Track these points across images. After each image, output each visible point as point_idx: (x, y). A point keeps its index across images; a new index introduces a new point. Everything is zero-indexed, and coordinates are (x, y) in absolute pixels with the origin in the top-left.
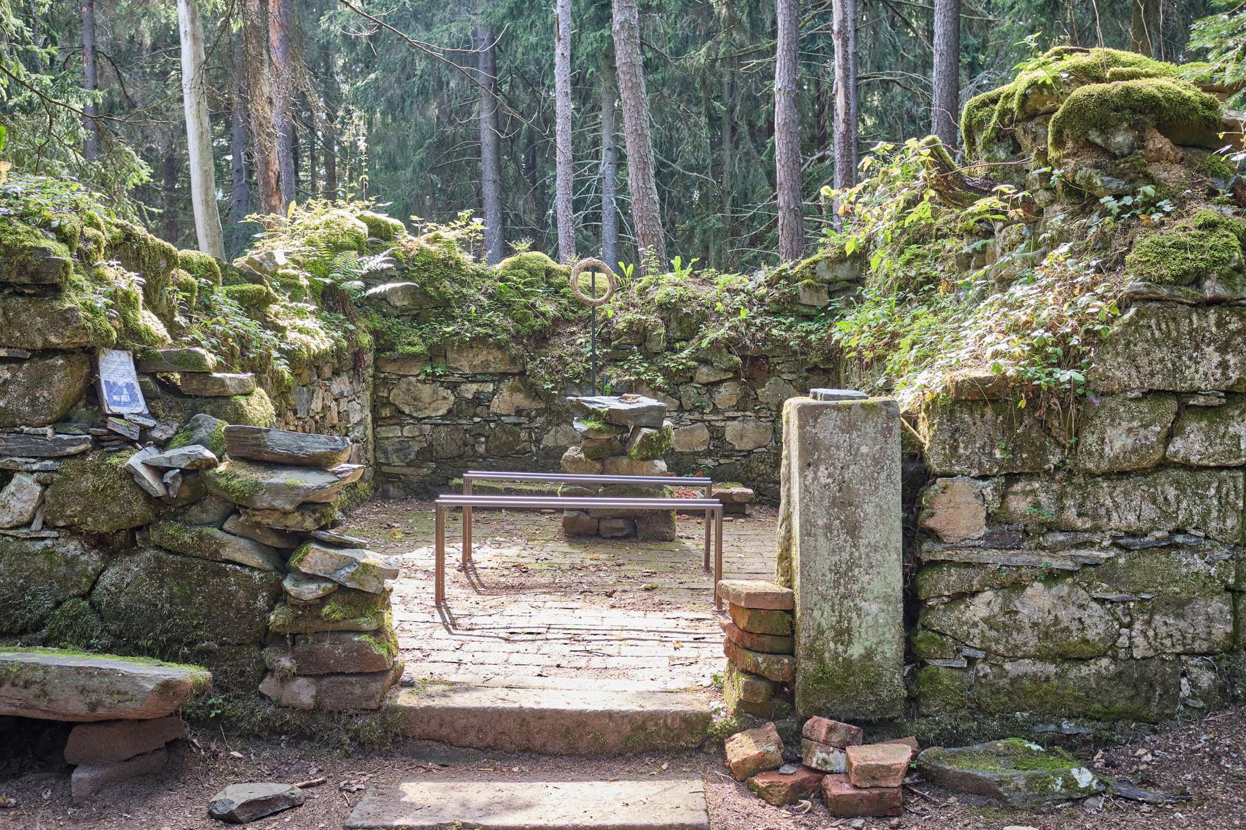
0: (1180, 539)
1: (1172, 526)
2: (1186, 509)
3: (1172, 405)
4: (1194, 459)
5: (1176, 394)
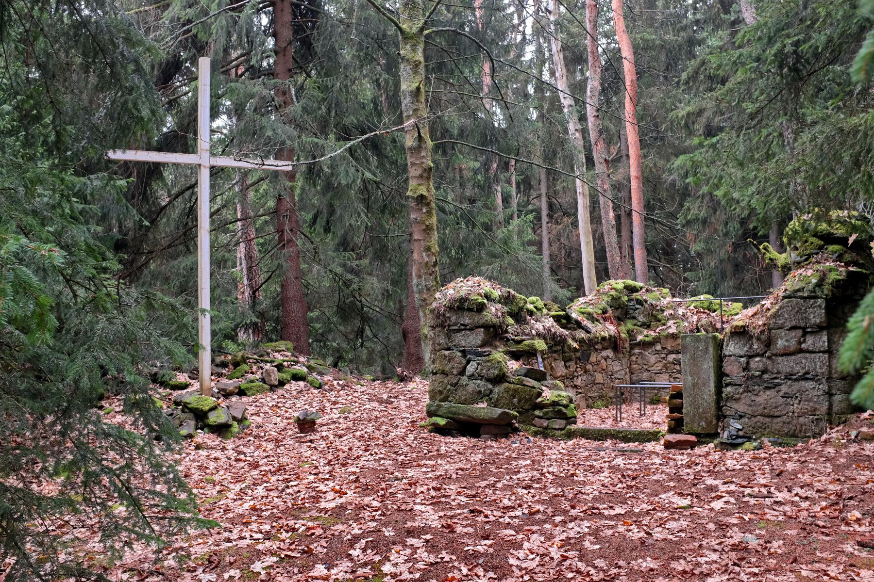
0: (808, 376)
2: (808, 366)
5: (800, 328)
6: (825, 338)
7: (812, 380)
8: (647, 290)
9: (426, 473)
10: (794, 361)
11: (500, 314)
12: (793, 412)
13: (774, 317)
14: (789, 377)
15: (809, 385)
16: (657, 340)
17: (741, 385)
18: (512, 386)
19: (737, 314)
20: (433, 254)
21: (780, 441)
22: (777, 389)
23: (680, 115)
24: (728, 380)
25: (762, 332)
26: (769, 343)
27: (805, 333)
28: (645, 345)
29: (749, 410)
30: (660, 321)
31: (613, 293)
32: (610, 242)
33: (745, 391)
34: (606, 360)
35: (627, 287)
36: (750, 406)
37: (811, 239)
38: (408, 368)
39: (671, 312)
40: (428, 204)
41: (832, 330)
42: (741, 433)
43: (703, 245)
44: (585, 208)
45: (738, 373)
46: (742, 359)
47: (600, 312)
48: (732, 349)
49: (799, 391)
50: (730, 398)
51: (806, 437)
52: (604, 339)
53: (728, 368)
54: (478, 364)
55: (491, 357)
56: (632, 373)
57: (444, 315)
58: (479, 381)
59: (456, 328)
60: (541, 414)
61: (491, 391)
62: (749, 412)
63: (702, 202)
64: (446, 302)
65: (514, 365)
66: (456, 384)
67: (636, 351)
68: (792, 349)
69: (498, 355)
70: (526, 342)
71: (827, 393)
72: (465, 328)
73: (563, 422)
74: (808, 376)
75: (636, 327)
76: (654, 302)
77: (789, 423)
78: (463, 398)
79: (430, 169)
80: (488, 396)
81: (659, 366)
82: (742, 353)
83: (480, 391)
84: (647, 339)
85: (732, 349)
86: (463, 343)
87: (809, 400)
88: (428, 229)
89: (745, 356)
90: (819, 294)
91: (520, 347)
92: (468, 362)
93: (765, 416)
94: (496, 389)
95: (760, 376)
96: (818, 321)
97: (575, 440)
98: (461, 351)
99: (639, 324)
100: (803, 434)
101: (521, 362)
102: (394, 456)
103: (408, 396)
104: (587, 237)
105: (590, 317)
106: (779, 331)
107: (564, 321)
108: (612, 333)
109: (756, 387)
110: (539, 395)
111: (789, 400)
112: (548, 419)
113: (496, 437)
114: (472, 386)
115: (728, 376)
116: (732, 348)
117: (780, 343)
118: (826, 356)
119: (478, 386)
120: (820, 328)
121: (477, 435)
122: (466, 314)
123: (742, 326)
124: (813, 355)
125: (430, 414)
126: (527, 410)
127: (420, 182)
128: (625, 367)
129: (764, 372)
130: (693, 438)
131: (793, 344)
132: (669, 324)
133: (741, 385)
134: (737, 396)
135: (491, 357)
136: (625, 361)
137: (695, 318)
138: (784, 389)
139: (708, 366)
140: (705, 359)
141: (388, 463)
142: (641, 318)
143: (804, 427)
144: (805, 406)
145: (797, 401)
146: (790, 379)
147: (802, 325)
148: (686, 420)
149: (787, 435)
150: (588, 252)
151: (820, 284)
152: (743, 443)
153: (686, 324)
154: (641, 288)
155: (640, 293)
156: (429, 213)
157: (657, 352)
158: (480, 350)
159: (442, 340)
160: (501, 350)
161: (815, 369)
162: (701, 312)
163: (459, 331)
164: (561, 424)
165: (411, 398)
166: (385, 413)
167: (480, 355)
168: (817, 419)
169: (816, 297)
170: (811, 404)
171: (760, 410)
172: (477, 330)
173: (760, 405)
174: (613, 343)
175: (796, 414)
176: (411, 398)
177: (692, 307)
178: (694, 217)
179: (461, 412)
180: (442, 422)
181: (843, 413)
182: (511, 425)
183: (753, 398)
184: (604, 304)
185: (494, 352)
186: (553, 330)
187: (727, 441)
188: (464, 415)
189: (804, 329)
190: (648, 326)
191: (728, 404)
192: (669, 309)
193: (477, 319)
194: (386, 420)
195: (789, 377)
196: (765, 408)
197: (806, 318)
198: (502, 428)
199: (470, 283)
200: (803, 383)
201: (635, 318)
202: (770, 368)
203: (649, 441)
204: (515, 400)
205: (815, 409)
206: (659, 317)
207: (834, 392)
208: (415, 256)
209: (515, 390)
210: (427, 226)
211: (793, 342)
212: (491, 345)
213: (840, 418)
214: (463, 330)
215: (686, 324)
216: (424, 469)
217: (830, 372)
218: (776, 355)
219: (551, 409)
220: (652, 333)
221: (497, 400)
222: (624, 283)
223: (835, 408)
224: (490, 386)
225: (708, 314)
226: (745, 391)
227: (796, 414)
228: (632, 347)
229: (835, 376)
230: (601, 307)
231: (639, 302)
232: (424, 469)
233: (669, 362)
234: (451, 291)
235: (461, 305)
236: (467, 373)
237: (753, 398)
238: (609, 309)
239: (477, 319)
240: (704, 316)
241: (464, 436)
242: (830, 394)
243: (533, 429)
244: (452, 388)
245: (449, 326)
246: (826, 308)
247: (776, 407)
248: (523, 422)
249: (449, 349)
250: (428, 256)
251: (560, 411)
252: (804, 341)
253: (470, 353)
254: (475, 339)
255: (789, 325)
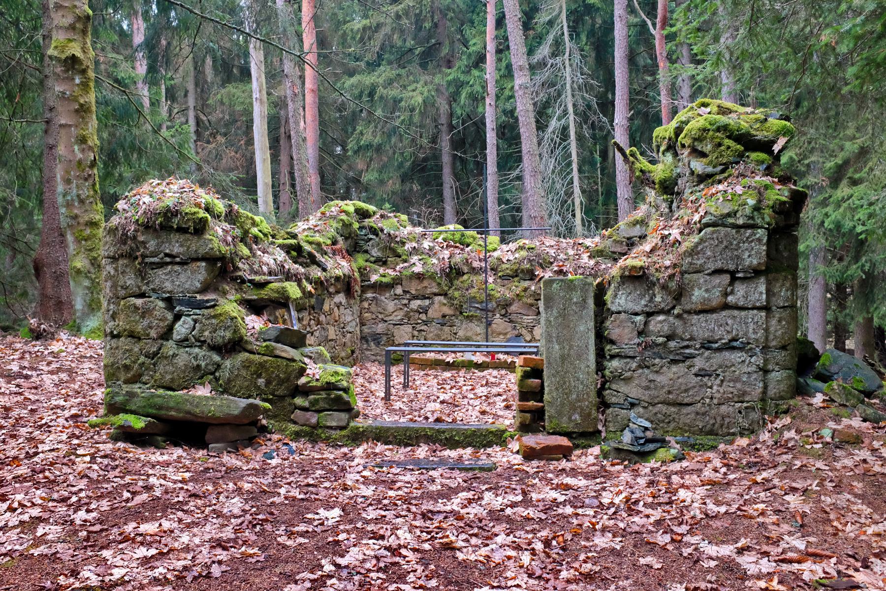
0: (735, 344)
1: (730, 337)
2: (736, 329)
3: (728, 276)
4: (741, 303)
5: (727, 271)
6: (763, 288)
7: (741, 349)
8: (382, 216)
9: (146, 562)
10: (716, 321)
11: (230, 239)
12: (712, 398)
13: (691, 255)
14: (707, 345)
15: (736, 357)
16: (397, 281)
17: (633, 358)
18: (256, 358)
19: (495, 250)
20: (91, 148)
21: (692, 441)
22: (687, 363)
23: (356, 28)
24: (615, 350)
25: (672, 277)
26: (679, 295)
27: (734, 279)
28: (381, 287)
29: (645, 396)
30: (400, 257)
31: (343, 217)
33: (640, 367)
34: (338, 307)
35: (358, 211)
36: (647, 388)
37: (728, 142)
38: (46, 318)
39: (414, 244)
40: (84, 72)
41: (771, 276)
42: (649, 434)
43: (376, 175)
44: (262, 117)
45: (630, 339)
46: (638, 318)
47: (329, 242)
48: (622, 302)
49: (720, 367)
50: (618, 377)
51: (729, 434)
53: (613, 329)
54: (195, 321)
55: (219, 310)
56: (362, 324)
57: (135, 238)
58: (197, 350)
59: (156, 260)
60: (306, 404)
61: (219, 366)
62: (646, 398)
63: (376, 127)
64: (138, 215)
65: (254, 323)
66: (155, 354)
67: (369, 295)
68: (714, 303)
69: (230, 305)
70: (271, 285)
71: (761, 369)
72: (172, 259)
73: (344, 416)
74: (735, 344)
75: (368, 264)
76: (392, 232)
77: (704, 414)
78: (168, 377)
79: (88, 17)
80: (213, 373)
81: (400, 315)
82: (638, 309)
83: (198, 366)
84: (384, 280)
85: (622, 302)
86: (168, 286)
87: (737, 380)
88: (83, 110)
89: (643, 312)
90: (759, 221)
91: (264, 293)
92: (177, 317)
93: (669, 404)
94: (228, 363)
95: (664, 345)
96: (755, 262)
97: (365, 446)
98: (163, 300)
99: (372, 259)
100: (725, 430)
101: (265, 317)
102: (62, 509)
103: (54, 366)
104: (264, 153)
106: (695, 276)
107: (294, 253)
108: (346, 271)
109: (657, 361)
110: (302, 372)
111: (706, 379)
112: (318, 411)
113: (235, 447)
114: (184, 358)
115: (612, 342)
116: (620, 300)
117: (698, 295)
118: (763, 314)
119: (196, 358)
120: (757, 273)
121: (203, 445)
122: (174, 237)
123: (642, 268)
124: (743, 313)
125: (114, 408)
126: (282, 398)
127: (70, 35)
128: (355, 316)
129: (670, 338)
130: (564, 441)
131: (716, 297)
132: (412, 261)
133: (633, 358)
134: (629, 374)
135: (219, 310)
136: (356, 308)
137: (446, 254)
138: (699, 363)
139: (586, 327)
140: (581, 317)
141: (53, 531)
142: (375, 253)
143: (727, 420)
144: (729, 388)
145: (718, 382)
146: (708, 349)
147: (732, 267)
148: (549, 411)
149: (701, 431)
150: (264, 172)
151: (757, 208)
152: (653, 452)
153: (435, 261)
154: (374, 213)
156: (85, 86)
157: (397, 297)
158: (199, 297)
159: (130, 280)
160: (232, 298)
161: (746, 334)
163: (162, 265)
164: (340, 420)
165: (59, 370)
166: (20, 398)
167: (200, 305)
168: (746, 408)
169: (754, 227)
170: (739, 385)
171: (662, 394)
172: (194, 265)
173: (663, 387)
174: (346, 285)
175: (715, 401)
176: (59, 370)
177: (440, 240)
179: (172, 404)
180: (138, 423)
181: (782, 398)
182: (255, 423)
183: (651, 376)
185: (221, 301)
186: (287, 267)
187: (631, 448)
188: (178, 410)
189: (733, 274)
191: (614, 387)
193: (195, 246)
194: (24, 413)
195: (707, 345)
196: (669, 392)
197: (738, 257)
198: (244, 432)
199: (175, 187)
200: (727, 354)
201: (366, 252)
202: (679, 331)
203: (489, 445)
204: (261, 381)
205: (745, 393)
206: (399, 251)
207: (770, 367)
208: (61, 150)
209: (262, 365)
210: (82, 105)
211: (717, 293)
212: (216, 290)
213: (777, 405)
214: (167, 264)
215: (435, 261)
216: (142, 552)
217: (767, 338)
218: (689, 312)
219: (324, 395)
220: (390, 272)
221: (229, 381)
223: (771, 392)
224: (216, 358)
225: (462, 250)
226: (640, 367)
227: (715, 401)
228: (364, 289)
229: (774, 343)
230: (329, 235)
231: (374, 231)
232: (142, 552)
233: (412, 310)
234: (147, 199)
235: (166, 222)
236: (176, 336)
237: (651, 376)
238: (340, 239)
239: (195, 246)
240: (458, 251)
241: (176, 444)
242: (765, 371)
243: (293, 428)
244: (148, 361)
245: (144, 256)
246: (768, 243)
247: (686, 391)
248: (274, 417)
249: (142, 295)
250: (83, 151)
251: (339, 399)
252: (732, 293)
253: (181, 302)
254: (190, 279)
255: (712, 266)
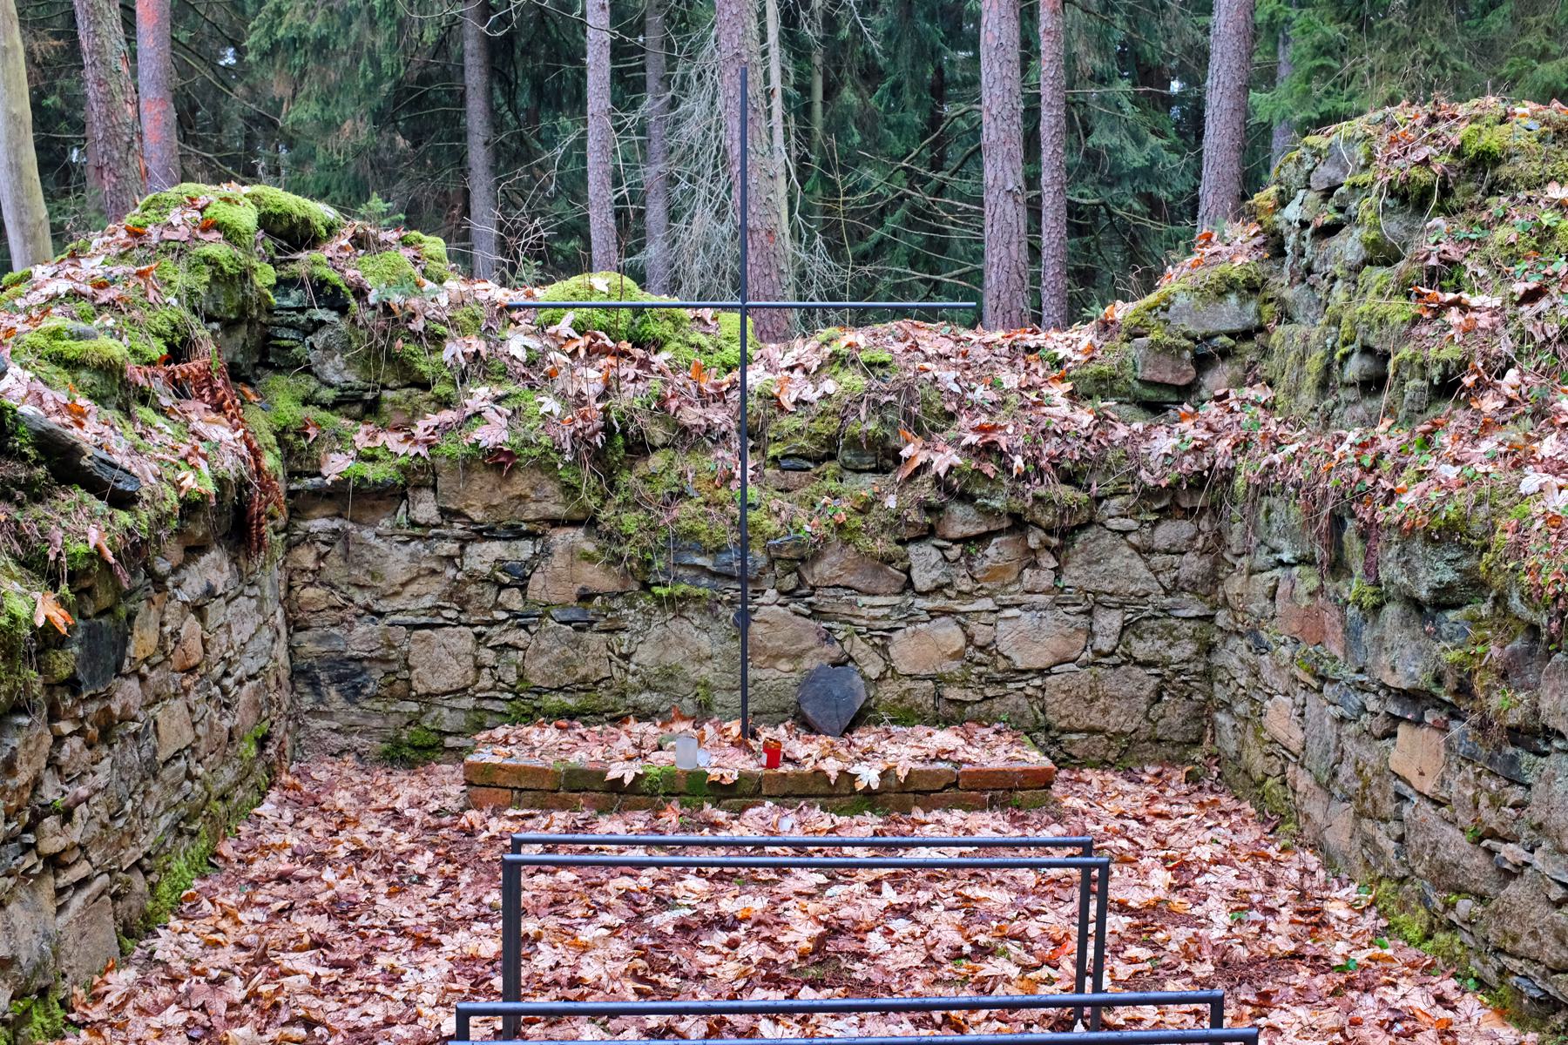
8: (359, 241)
16: (418, 477)
28: (356, 498)
30: (426, 386)
32: (98, 51)
35: (269, 222)
39: (477, 344)
47: (157, 349)
52: (191, 507)
56: (296, 625)
67: (319, 524)
75: (312, 412)
76: (396, 299)
81: (429, 593)
84: (374, 473)
99: (328, 395)
105: (117, 388)
108: (229, 465)
132: (472, 405)
142: (339, 372)
153: (551, 405)
155: (330, 249)
157: (419, 531)
162: (607, 352)
177: (564, 328)
178: (293, 34)
184: (171, 309)
190: (362, 405)
192: (463, 331)
206: (424, 366)
215: (551, 405)
220: (392, 440)
222: (256, 200)
230: (160, 321)
231: (331, 296)
233: (473, 577)
238: (202, 332)
